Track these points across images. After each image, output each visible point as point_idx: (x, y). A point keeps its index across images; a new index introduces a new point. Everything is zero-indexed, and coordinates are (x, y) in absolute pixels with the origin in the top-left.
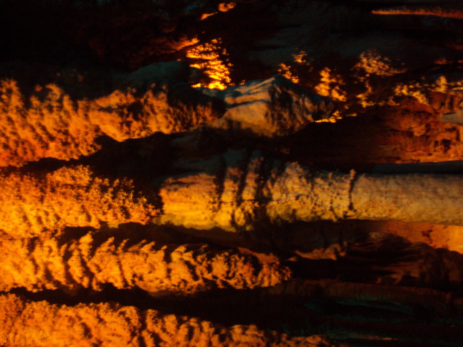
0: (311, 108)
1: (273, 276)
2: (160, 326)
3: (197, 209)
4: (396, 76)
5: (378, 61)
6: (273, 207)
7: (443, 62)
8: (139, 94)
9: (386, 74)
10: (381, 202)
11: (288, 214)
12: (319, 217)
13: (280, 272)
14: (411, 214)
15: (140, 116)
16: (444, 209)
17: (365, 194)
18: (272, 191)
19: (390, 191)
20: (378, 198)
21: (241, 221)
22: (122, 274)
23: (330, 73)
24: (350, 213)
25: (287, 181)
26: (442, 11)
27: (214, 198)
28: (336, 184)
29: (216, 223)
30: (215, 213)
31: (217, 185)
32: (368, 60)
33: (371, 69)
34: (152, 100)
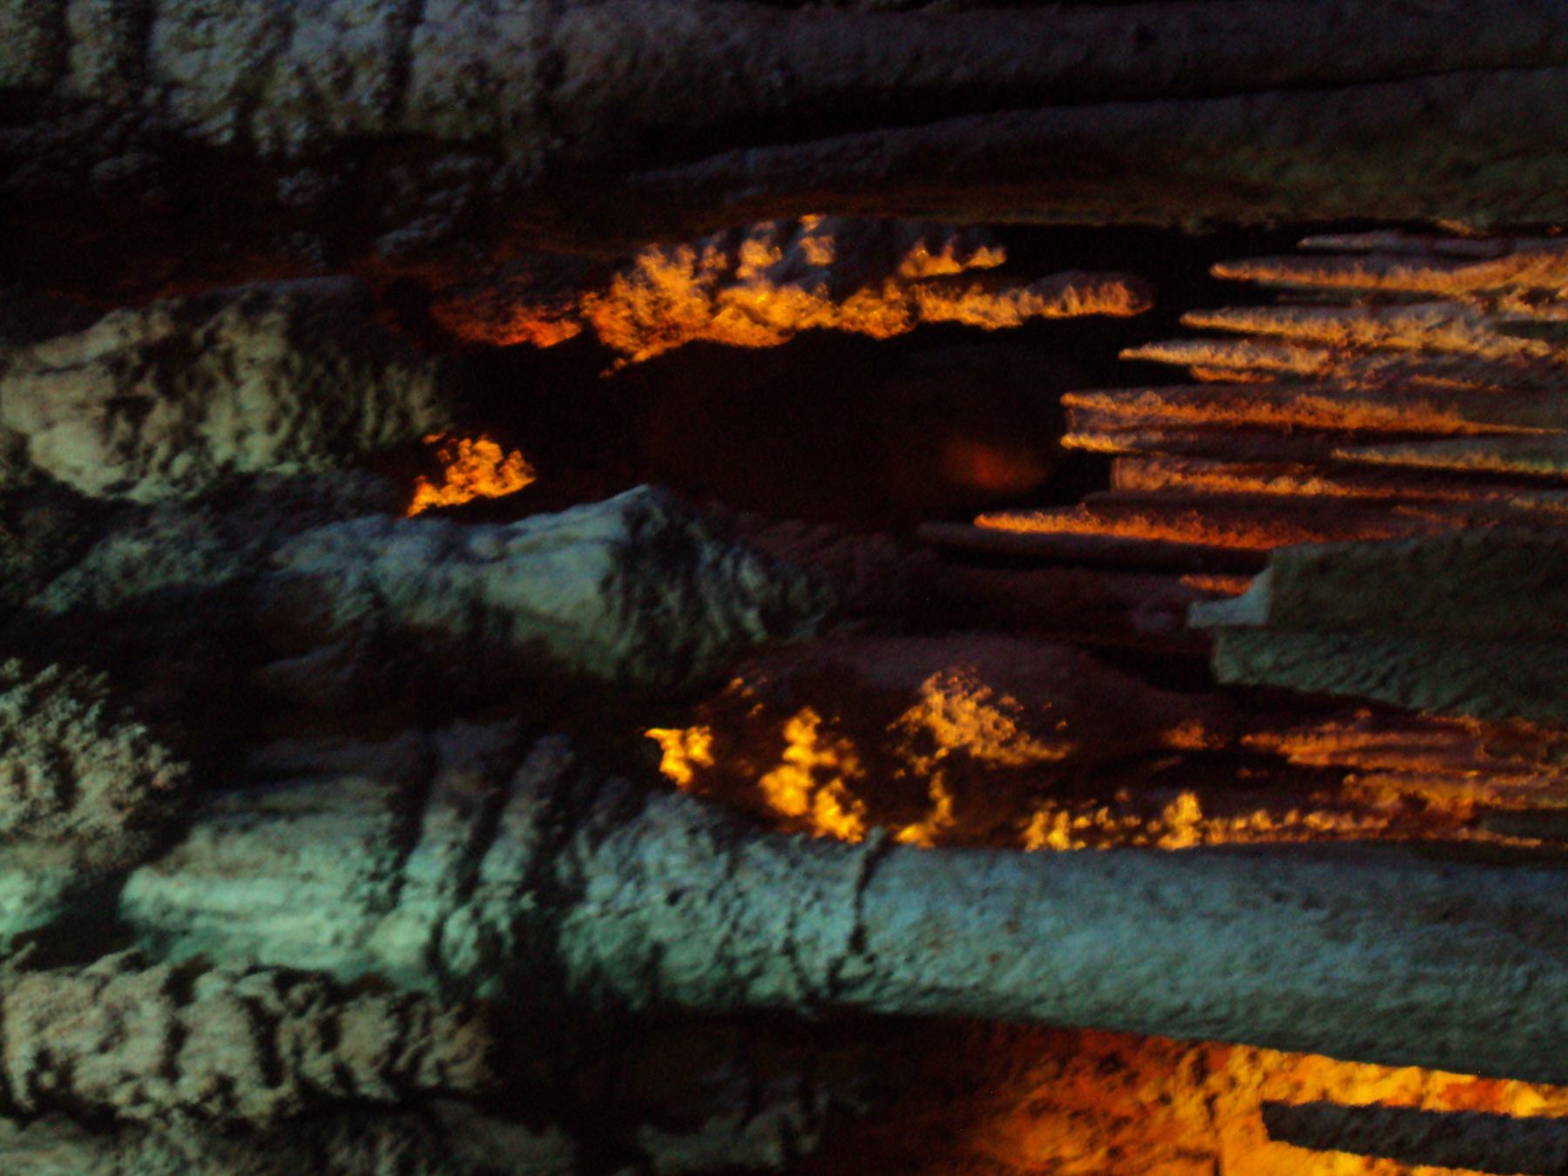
0: (760, 588)
3: (311, 901)
4: (1036, 768)
5: (981, 704)
6: (586, 929)
7: (1189, 738)
8: (198, 310)
12: (743, 984)
15: (180, 381)
16: (1179, 959)
18: (590, 869)
19: (998, 890)
20: (954, 910)
21: (464, 958)
23: (819, 730)
25: (645, 839)
26: (1204, 524)
27: (380, 861)
28: (818, 865)
29: (373, 957)
30: (373, 917)
32: (947, 697)
34: (233, 334)
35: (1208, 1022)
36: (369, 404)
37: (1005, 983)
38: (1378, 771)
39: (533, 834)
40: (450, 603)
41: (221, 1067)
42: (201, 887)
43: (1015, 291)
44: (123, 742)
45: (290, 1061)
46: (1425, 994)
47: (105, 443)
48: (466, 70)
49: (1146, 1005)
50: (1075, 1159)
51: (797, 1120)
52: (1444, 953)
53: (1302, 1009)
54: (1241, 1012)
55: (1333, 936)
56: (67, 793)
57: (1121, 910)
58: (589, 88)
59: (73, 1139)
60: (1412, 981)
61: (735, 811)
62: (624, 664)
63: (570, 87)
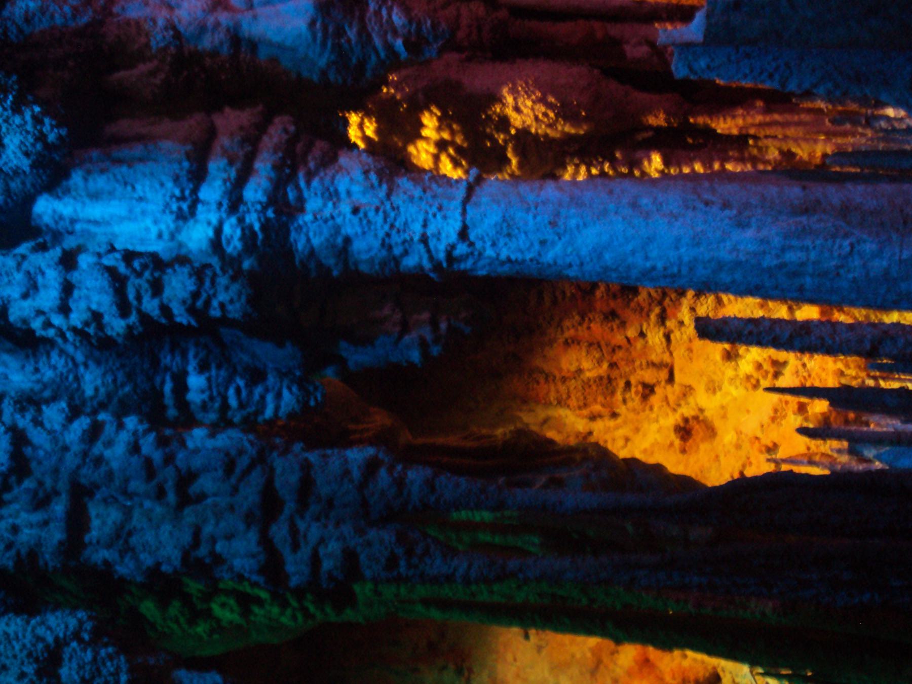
0: (404, 26)
1: (286, 393)
2: (29, 416)
3: (144, 213)
4: (568, 139)
5: (534, 102)
7: (658, 120)
9: (549, 131)
11: (334, 246)
13: (301, 387)
14: (584, 252)
17: (495, 207)
18: (306, 194)
20: (519, 215)
23: (440, 119)
24: (461, 249)
27: (182, 191)
28: (440, 191)
29: (181, 245)
30: (181, 223)
33: (518, 117)
35: (665, 277)
37: (549, 256)
38: (766, 137)
39: (273, 175)
40: (220, 36)
41: (94, 307)
42: (79, 207)
44: (28, 115)
45: (135, 303)
46: (791, 257)
49: (629, 268)
50: (589, 370)
51: (429, 337)
52: (805, 232)
53: (720, 266)
54: (684, 270)
59: (9, 351)
60: (783, 250)
61: (391, 160)
62: (324, 73)
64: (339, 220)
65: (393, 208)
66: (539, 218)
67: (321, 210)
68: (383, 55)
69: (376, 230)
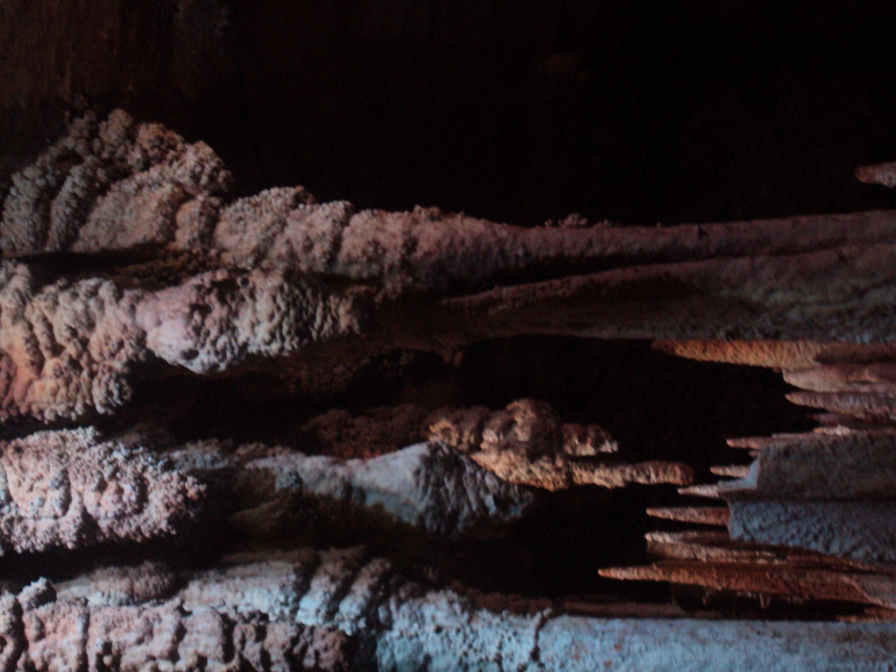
0: (495, 487)
10: (593, 646)
11: (415, 662)
15: (228, 297)
17: (566, 633)
18: (395, 616)
20: (587, 639)
22: (84, 642)
27: (287, 598)
31: (298, 577)
36: (319, 311)
40: (336, 483)
41: (201, 650)
43: (622, 468)
47: (186, 326)
48: (369, 243)
55: (788, 650)
56: (143, 498)
57: (676, 640)
58: (428, 254)
62: (422, 518)
63: (419, 253)
64: (422, 639)
65: (472, 631)
66: (605, 643)
67: (407, 630)
68: (474, 507)
69: (455, 649)
